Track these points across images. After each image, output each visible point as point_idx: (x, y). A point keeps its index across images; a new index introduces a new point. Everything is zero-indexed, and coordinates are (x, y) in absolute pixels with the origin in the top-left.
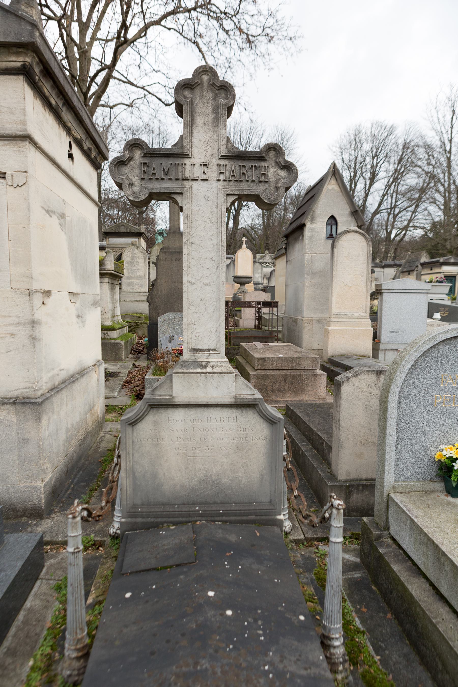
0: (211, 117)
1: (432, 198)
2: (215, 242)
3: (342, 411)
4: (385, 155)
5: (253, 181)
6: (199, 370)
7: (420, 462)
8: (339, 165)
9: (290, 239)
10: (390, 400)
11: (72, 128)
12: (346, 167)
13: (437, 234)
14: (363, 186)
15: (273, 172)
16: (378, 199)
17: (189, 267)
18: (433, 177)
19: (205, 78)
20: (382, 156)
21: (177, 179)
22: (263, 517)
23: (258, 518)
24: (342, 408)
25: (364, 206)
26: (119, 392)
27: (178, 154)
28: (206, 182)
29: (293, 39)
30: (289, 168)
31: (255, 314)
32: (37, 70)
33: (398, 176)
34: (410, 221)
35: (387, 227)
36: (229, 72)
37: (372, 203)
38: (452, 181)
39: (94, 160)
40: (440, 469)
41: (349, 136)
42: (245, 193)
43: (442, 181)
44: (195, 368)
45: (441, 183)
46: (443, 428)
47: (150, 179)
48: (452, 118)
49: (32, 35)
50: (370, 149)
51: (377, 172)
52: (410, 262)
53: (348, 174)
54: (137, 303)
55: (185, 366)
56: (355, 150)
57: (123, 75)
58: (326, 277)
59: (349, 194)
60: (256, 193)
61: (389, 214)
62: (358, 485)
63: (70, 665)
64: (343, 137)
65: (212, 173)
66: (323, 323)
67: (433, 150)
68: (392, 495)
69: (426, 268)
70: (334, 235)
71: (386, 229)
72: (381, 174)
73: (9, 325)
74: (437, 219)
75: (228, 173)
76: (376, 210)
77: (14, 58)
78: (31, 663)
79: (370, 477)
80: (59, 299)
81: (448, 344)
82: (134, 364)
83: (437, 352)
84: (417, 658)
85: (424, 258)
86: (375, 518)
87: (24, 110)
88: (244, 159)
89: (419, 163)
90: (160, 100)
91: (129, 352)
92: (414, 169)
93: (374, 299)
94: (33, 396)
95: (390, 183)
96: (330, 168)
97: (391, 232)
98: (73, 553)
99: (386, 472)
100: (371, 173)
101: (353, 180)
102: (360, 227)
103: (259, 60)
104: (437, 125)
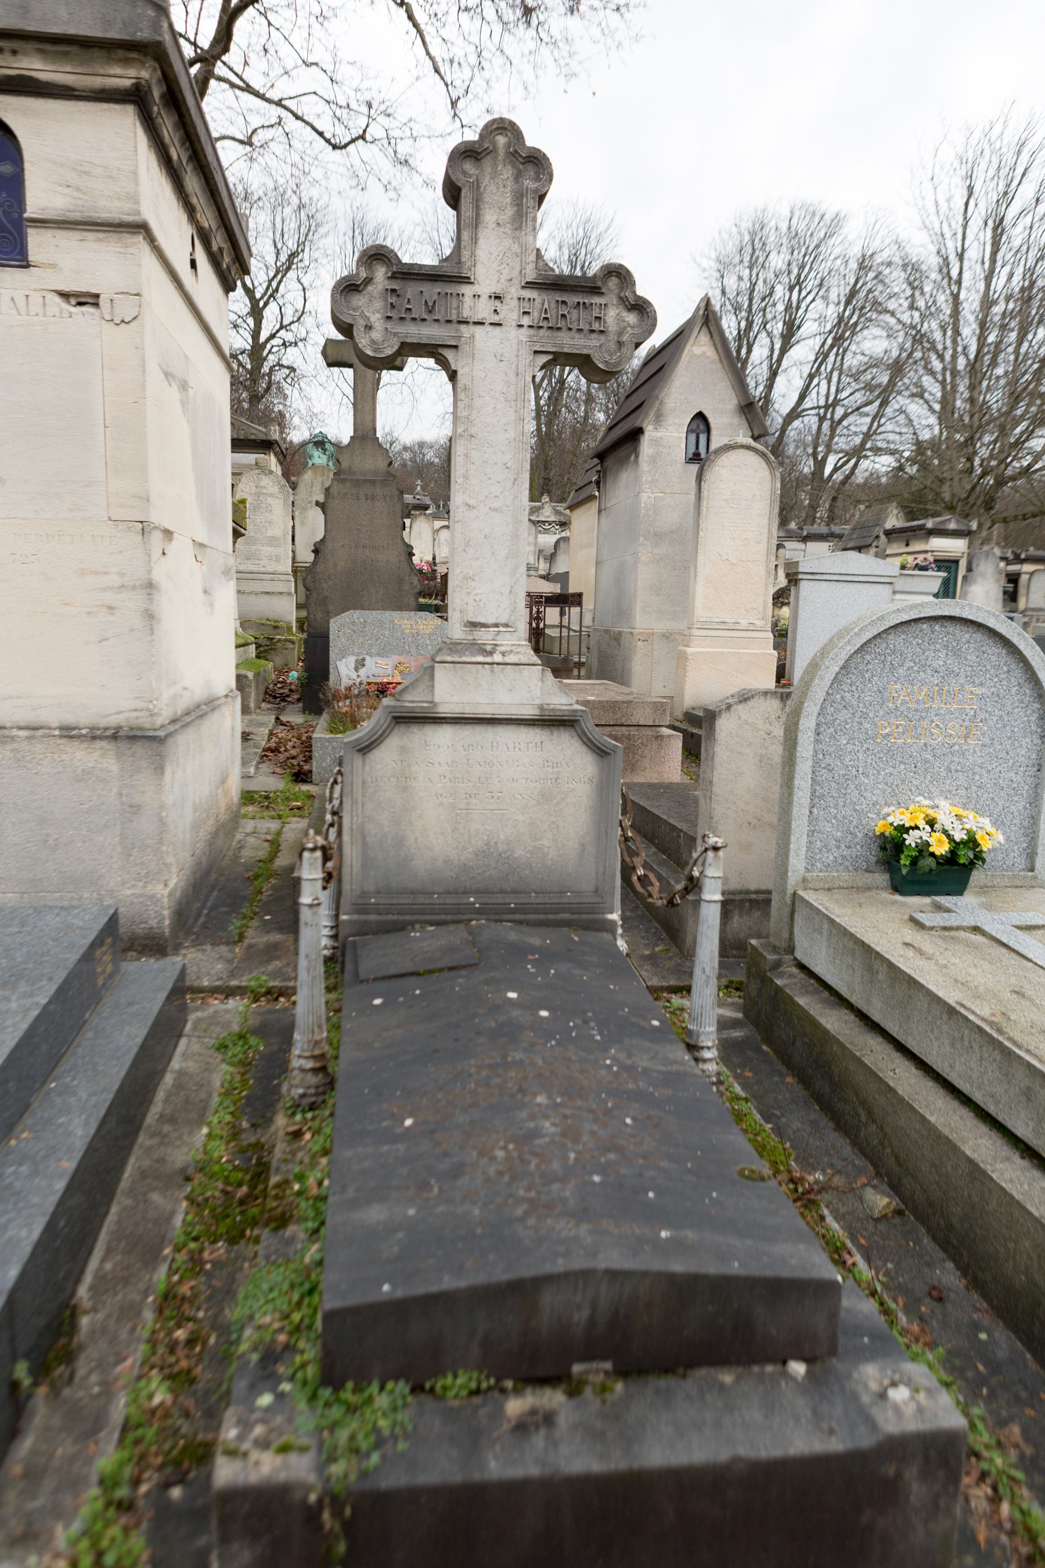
0: (510, 211)
1: (916, 385)
2: (511, 435)
3: (717, 765)
4: (817, 282)
5: (580, 330)
6: (480, 659)
7: (850, 838)
8: (716, 304)
9: (609, 462)
10: (801, 727)
11: (198, 207)
12: (729, 307)
13: (924, 467)
14: (766, 352)
15: (614, 315)
16: (799, 384)
17: (466, 477)
18: (919, 338)
19: (501, 140)
20: (811, 284)
21: (449, 321)
22: (584, 916)
23: (576, 917)
24: (717, 759)
25: (767, 398)
26: (257, 768)
27: (449, 276)
28: (498, 328)
29: (623, 10)
30: (641, 308)
31: (530, 624)
32: (156, 93)
33: (844, 332)
34: (867, 436)
35: (815, 448)
36: (478, 80)
37: (785, 394)
38: (960, 349)
39: (226, 273)
40: (883, 848)
41: (739, 233)
42: (566, 350)
43: (940, 347)
44: (473, 655)
45: (937, 352)
46: (890, 780)
47: (402, 319)
48: (967, 204)
49: (156, 27)
50: (784, 267)
51: (797, 322)
52: (862, 527)
53: (734, 324)
54: (267, 597)
55: (457, 651)
56: (751, 268)
57: (231, 69)
58: (684, 543)
59: (735, 365)
60: (585, 352)
61: (822, 419)
62: (742, 901)
63: (302, 1080)
64: (725, 236)
65: (510, 312)
66: (674, 641)
67: (923, 276)
68: (801, 893)
69: (896, 540)
70: (703, 455)
71: (815, 454)
72: (809, 328)
73: (104, 589)
74: (925, 435)
75: (536, 314)
76: (794, 409)
77: (118, 71)
78: (205, 1130)
79: (763, 887)
80: (181, 547)
81: (904, 632)
82: (277, 719)
83: (884, 645)
84: (831, 1124)
85: (894, 520)
86: (772, 939)
87: (135, 173)
88: (566, 290)
89: (892, 305)
90: (321, 134)
91: (262, 696)
92: (881, 317)
93: (783, 604)
94: (148, 726)
95: (826, 347)
96: (698, 309)
97: (824, 460)
98: (311, 906)
99: (792, 853)
100: (785, 323)
101: (745, 337)
102: (755, 438)
103: (545, 51)
104: (934, 218)
